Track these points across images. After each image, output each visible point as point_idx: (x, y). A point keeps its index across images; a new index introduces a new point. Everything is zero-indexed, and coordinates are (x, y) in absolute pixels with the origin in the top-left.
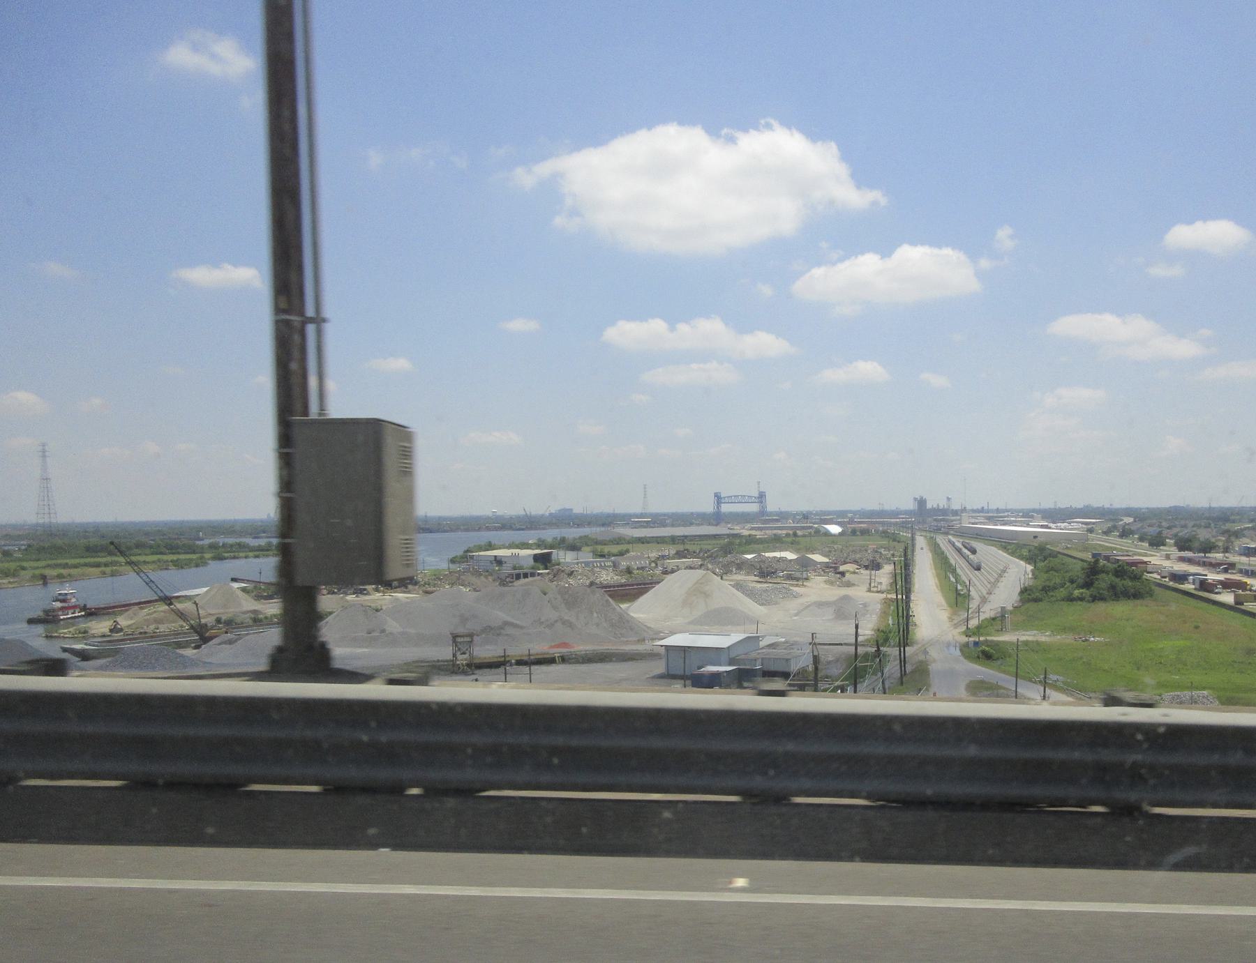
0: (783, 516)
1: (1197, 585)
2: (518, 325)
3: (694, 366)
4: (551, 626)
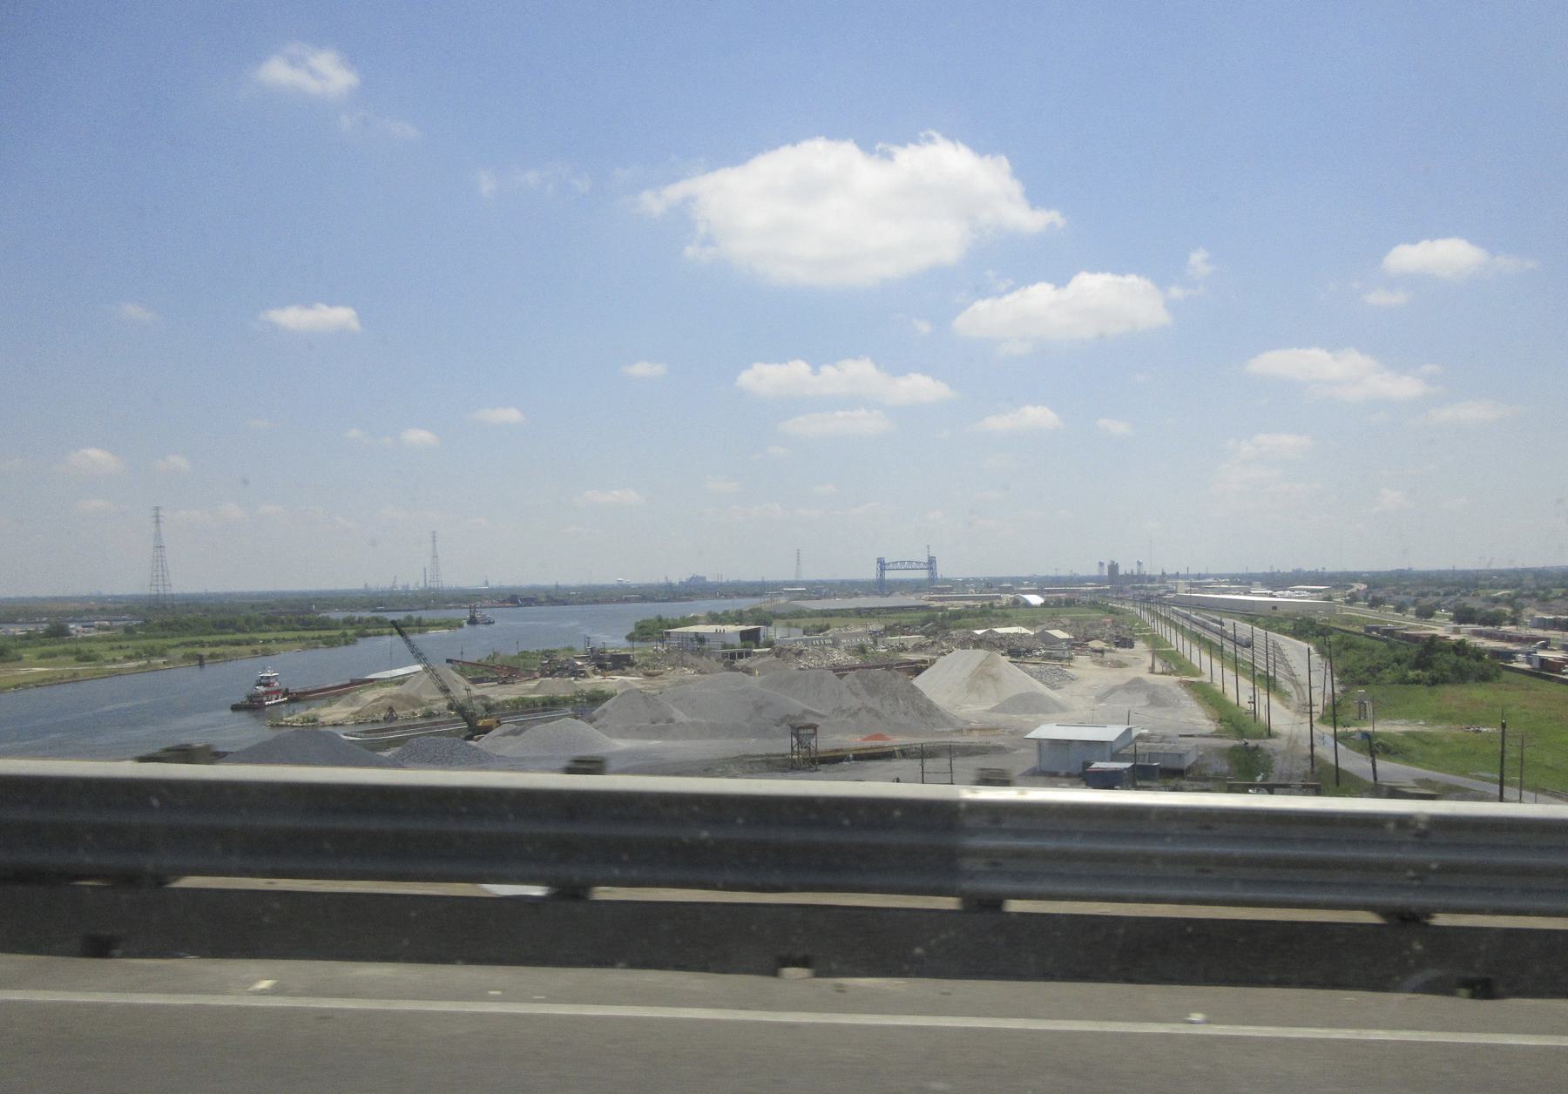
0: (954, 585)
1: (1537, 665)
2: (641, 369)
3: (840, 414)
4: (854, 714)
